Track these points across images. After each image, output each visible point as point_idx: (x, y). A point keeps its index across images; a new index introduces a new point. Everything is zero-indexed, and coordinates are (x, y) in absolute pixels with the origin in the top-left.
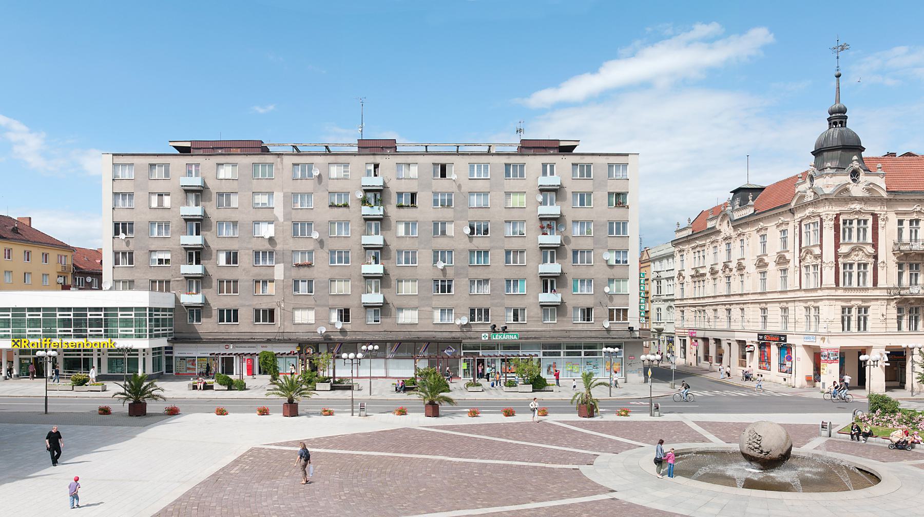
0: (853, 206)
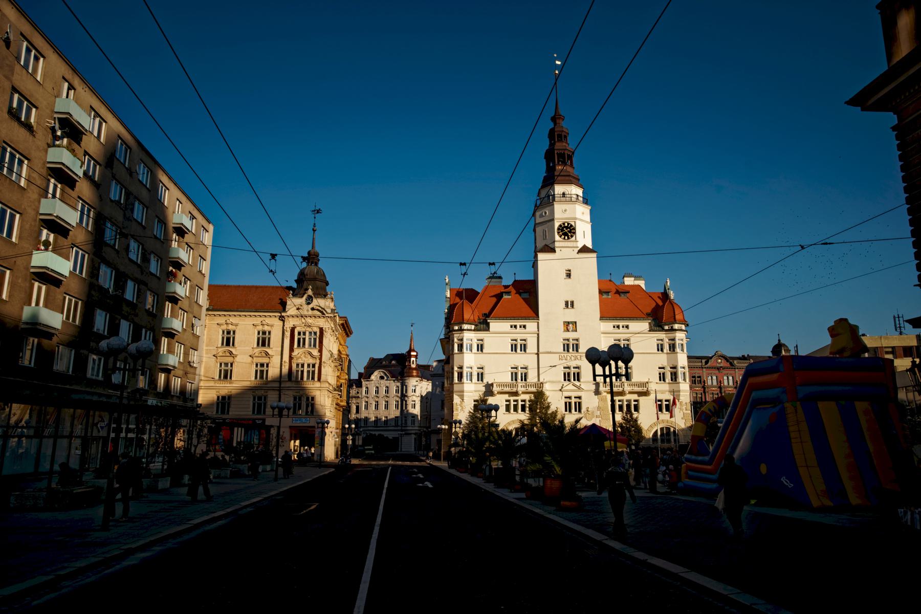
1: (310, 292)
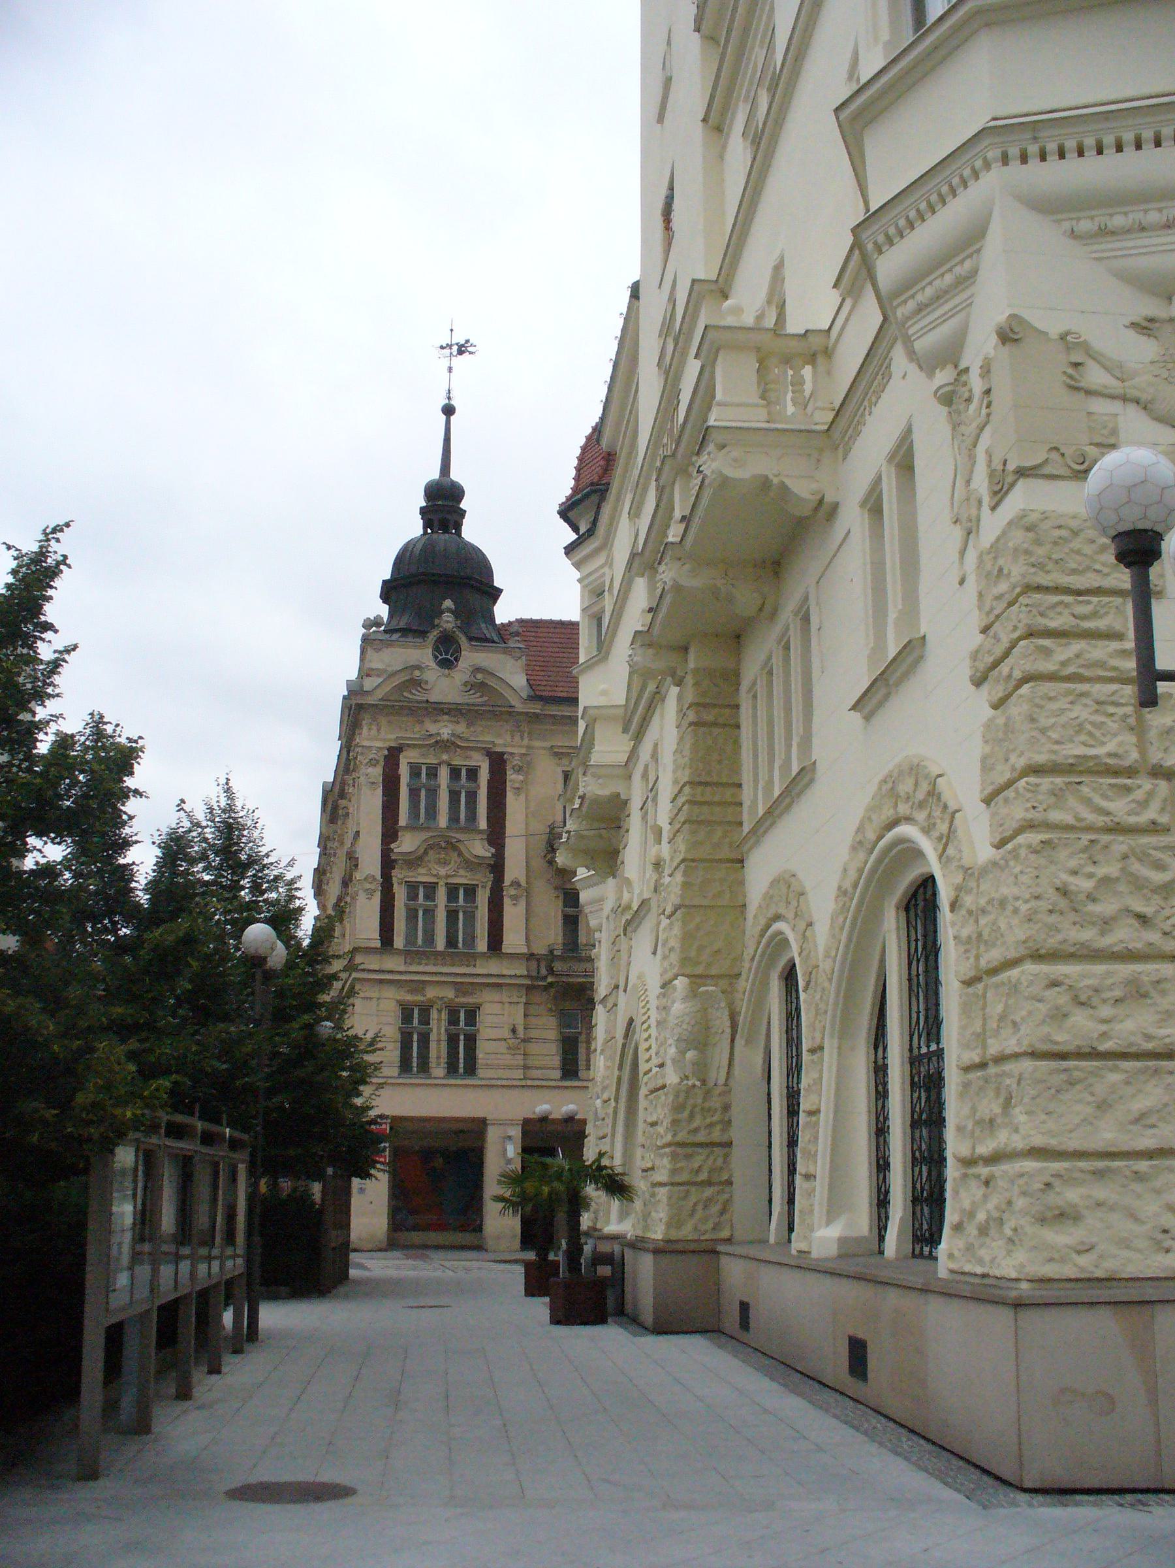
0: (432, 728)
1: (448, 621)
